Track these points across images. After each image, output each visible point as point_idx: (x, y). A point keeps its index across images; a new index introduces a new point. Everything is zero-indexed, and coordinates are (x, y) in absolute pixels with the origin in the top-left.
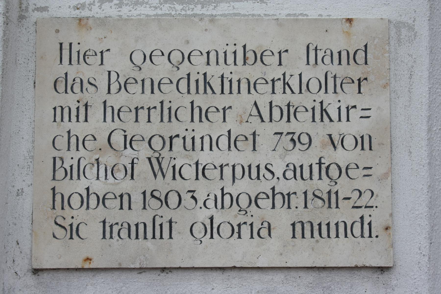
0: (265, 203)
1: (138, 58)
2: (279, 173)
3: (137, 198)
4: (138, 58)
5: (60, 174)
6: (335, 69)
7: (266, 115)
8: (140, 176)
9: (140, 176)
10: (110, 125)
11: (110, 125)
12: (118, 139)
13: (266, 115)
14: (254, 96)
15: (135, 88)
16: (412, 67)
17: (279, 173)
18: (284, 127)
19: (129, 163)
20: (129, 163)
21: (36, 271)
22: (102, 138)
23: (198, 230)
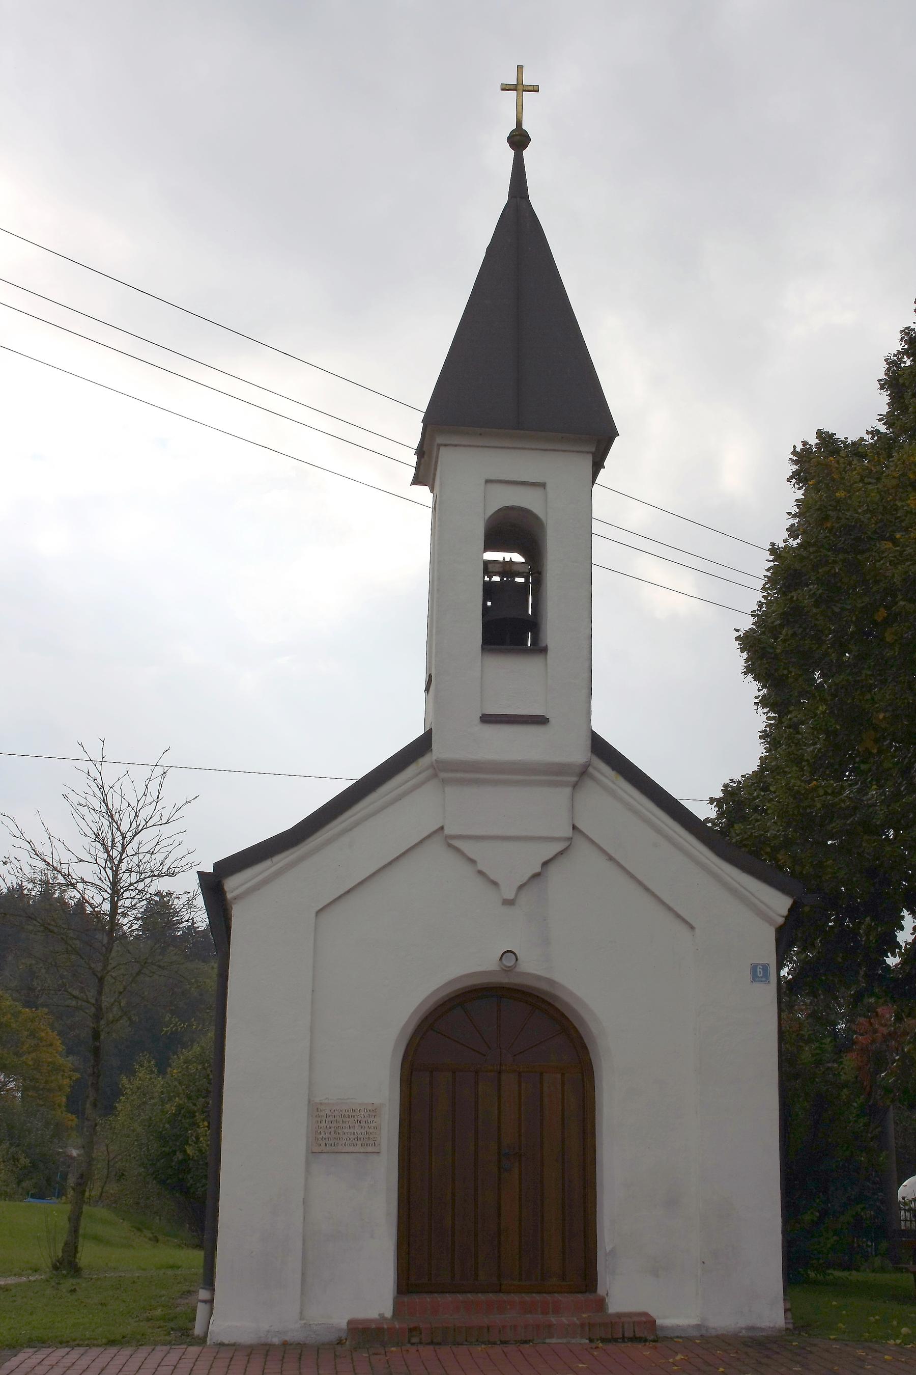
0: (356, 1140)
1: (332, 1111)
2: (359, 1133)
3: (332, 1139)
4: (332, 1111)
5: (317, 1134)
6: (370, 1113)
7: (356, 1122)
8: (210, 1092)
9: (210, 1092)
10: (326, 1124)
11: (326, 1124)
12: (328, 1127)
13: (356, 1122)
14: (354, 1119)
15: (331, 1117)
16: (75, 1243)
17: (359, 1133)
18: (360, 1125)
19: (520, 68)
20: (520, 68)
21: (313, 1152)
22: (325, 1127)
23: (343, 1145)
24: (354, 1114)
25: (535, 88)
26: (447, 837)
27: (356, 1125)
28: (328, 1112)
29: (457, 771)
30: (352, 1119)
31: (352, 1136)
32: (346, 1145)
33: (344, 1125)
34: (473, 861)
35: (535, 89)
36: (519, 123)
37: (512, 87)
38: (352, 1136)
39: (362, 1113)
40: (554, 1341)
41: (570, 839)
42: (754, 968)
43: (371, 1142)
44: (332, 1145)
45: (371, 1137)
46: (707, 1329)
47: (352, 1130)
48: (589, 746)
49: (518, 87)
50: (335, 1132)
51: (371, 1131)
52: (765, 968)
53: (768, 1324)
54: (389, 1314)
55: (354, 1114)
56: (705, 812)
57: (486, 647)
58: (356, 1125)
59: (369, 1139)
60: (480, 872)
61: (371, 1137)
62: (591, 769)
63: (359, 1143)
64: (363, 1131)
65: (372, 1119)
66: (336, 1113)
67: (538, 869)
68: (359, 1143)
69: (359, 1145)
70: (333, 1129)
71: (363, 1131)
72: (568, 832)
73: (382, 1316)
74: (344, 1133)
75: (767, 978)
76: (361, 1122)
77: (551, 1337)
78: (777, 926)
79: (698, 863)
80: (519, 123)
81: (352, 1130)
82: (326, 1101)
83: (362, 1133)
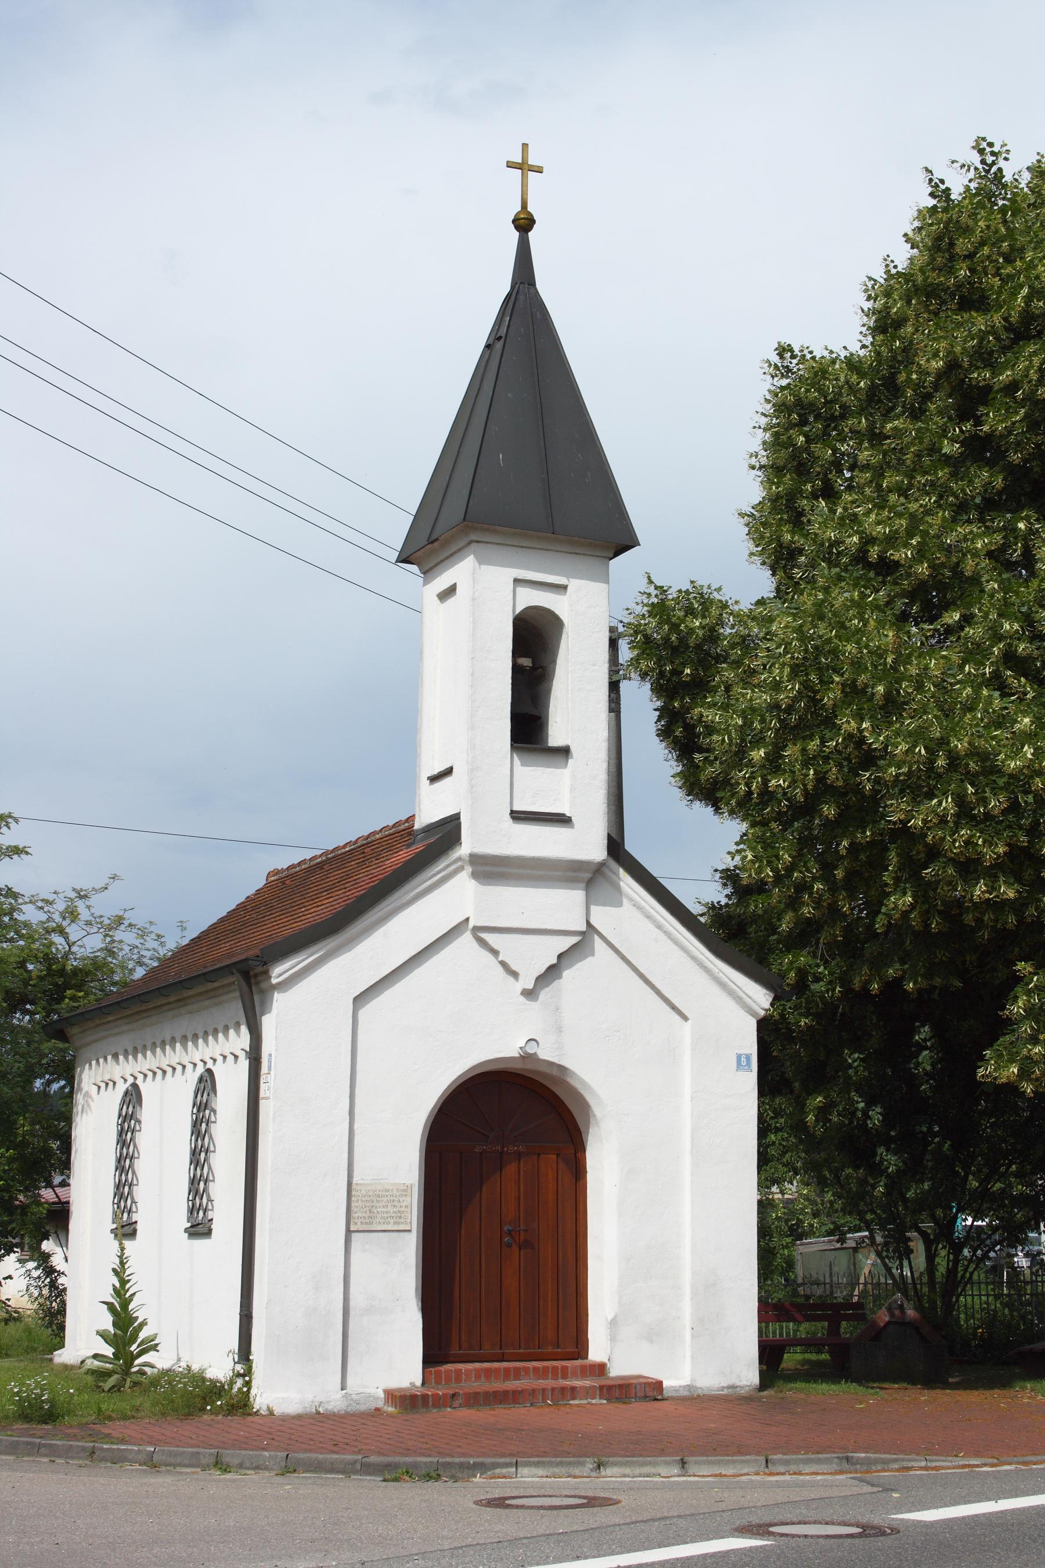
19: (525, 146)
20: (525, 146)
24: (387, 1194)
25: (540, 170)
26: (476, 929)
27: (389, 1205)
28: (363, 1192)
29: (486, 864)
30: (385, 1199)
31: (386, 1215)
32: (380, 1223)
33: (378, 1204)
34: (495, 952)
35: (539, 170)
36: (524, 205)
37: (518, 166)
38: (386, 1215)
39: (395, 1192)
40: (576, 1402)
41: (582, 933)
42: (739, 1057)
43: (402, 1220)
44: (366, 1223)
45: (403, 1215)
46: (696, 1388)
47: (385, 1210)
48: (606, 845)
49: (523, 167)
50: (370, 1211)
51: (402, 1209)
52: (748, 1057)
53: (745, 1383)
54: (418, 1382)
55: (387, 1194)
56: (695, 909)
57: (515, 745)
58: (389, 1205)
59: (400, 1217)
60: (503, 964)
61: (403, 1215)
62: (604, 869)
63: (392, 1221)
64: (395, 1210)
65: (404, 1198)
66: (371, 1193)
67: (555, 961)
68: (392, 1221)
69: (359, 1223)
70: (368, 1209)
71: (395, 1210)
72: (583, 927)
73: (412, 1384)
74: (378, 1212)
75: (749, 1067)
76: (393, 1201)
77: (573, 1399)
78: (759, 1018)
79: (694, 958)
80: (524, 205)
81: (385, 1210)
82: (362, 1182)
83: (395, 1212)
